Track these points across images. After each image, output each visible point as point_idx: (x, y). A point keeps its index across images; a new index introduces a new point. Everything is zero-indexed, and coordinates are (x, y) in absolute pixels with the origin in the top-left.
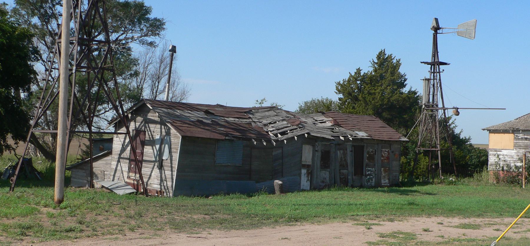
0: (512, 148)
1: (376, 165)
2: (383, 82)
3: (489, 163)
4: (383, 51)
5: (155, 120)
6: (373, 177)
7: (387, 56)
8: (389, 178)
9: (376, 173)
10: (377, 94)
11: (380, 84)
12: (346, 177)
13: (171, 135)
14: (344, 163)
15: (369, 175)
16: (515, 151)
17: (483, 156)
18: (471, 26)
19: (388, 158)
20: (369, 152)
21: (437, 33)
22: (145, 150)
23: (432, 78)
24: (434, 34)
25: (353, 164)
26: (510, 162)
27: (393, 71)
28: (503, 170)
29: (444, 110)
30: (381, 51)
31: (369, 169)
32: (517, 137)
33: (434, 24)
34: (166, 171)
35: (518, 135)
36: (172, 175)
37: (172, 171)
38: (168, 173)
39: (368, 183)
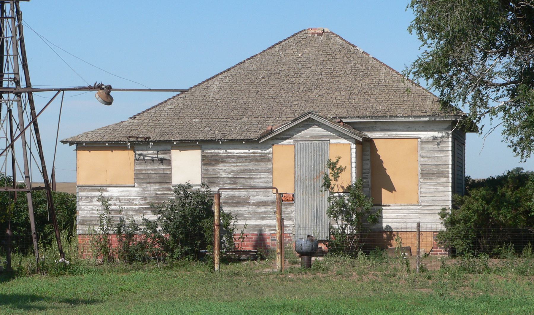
0: (131, 182)
3: (79, 218)
16: (137, 189)
32: (142, 157)
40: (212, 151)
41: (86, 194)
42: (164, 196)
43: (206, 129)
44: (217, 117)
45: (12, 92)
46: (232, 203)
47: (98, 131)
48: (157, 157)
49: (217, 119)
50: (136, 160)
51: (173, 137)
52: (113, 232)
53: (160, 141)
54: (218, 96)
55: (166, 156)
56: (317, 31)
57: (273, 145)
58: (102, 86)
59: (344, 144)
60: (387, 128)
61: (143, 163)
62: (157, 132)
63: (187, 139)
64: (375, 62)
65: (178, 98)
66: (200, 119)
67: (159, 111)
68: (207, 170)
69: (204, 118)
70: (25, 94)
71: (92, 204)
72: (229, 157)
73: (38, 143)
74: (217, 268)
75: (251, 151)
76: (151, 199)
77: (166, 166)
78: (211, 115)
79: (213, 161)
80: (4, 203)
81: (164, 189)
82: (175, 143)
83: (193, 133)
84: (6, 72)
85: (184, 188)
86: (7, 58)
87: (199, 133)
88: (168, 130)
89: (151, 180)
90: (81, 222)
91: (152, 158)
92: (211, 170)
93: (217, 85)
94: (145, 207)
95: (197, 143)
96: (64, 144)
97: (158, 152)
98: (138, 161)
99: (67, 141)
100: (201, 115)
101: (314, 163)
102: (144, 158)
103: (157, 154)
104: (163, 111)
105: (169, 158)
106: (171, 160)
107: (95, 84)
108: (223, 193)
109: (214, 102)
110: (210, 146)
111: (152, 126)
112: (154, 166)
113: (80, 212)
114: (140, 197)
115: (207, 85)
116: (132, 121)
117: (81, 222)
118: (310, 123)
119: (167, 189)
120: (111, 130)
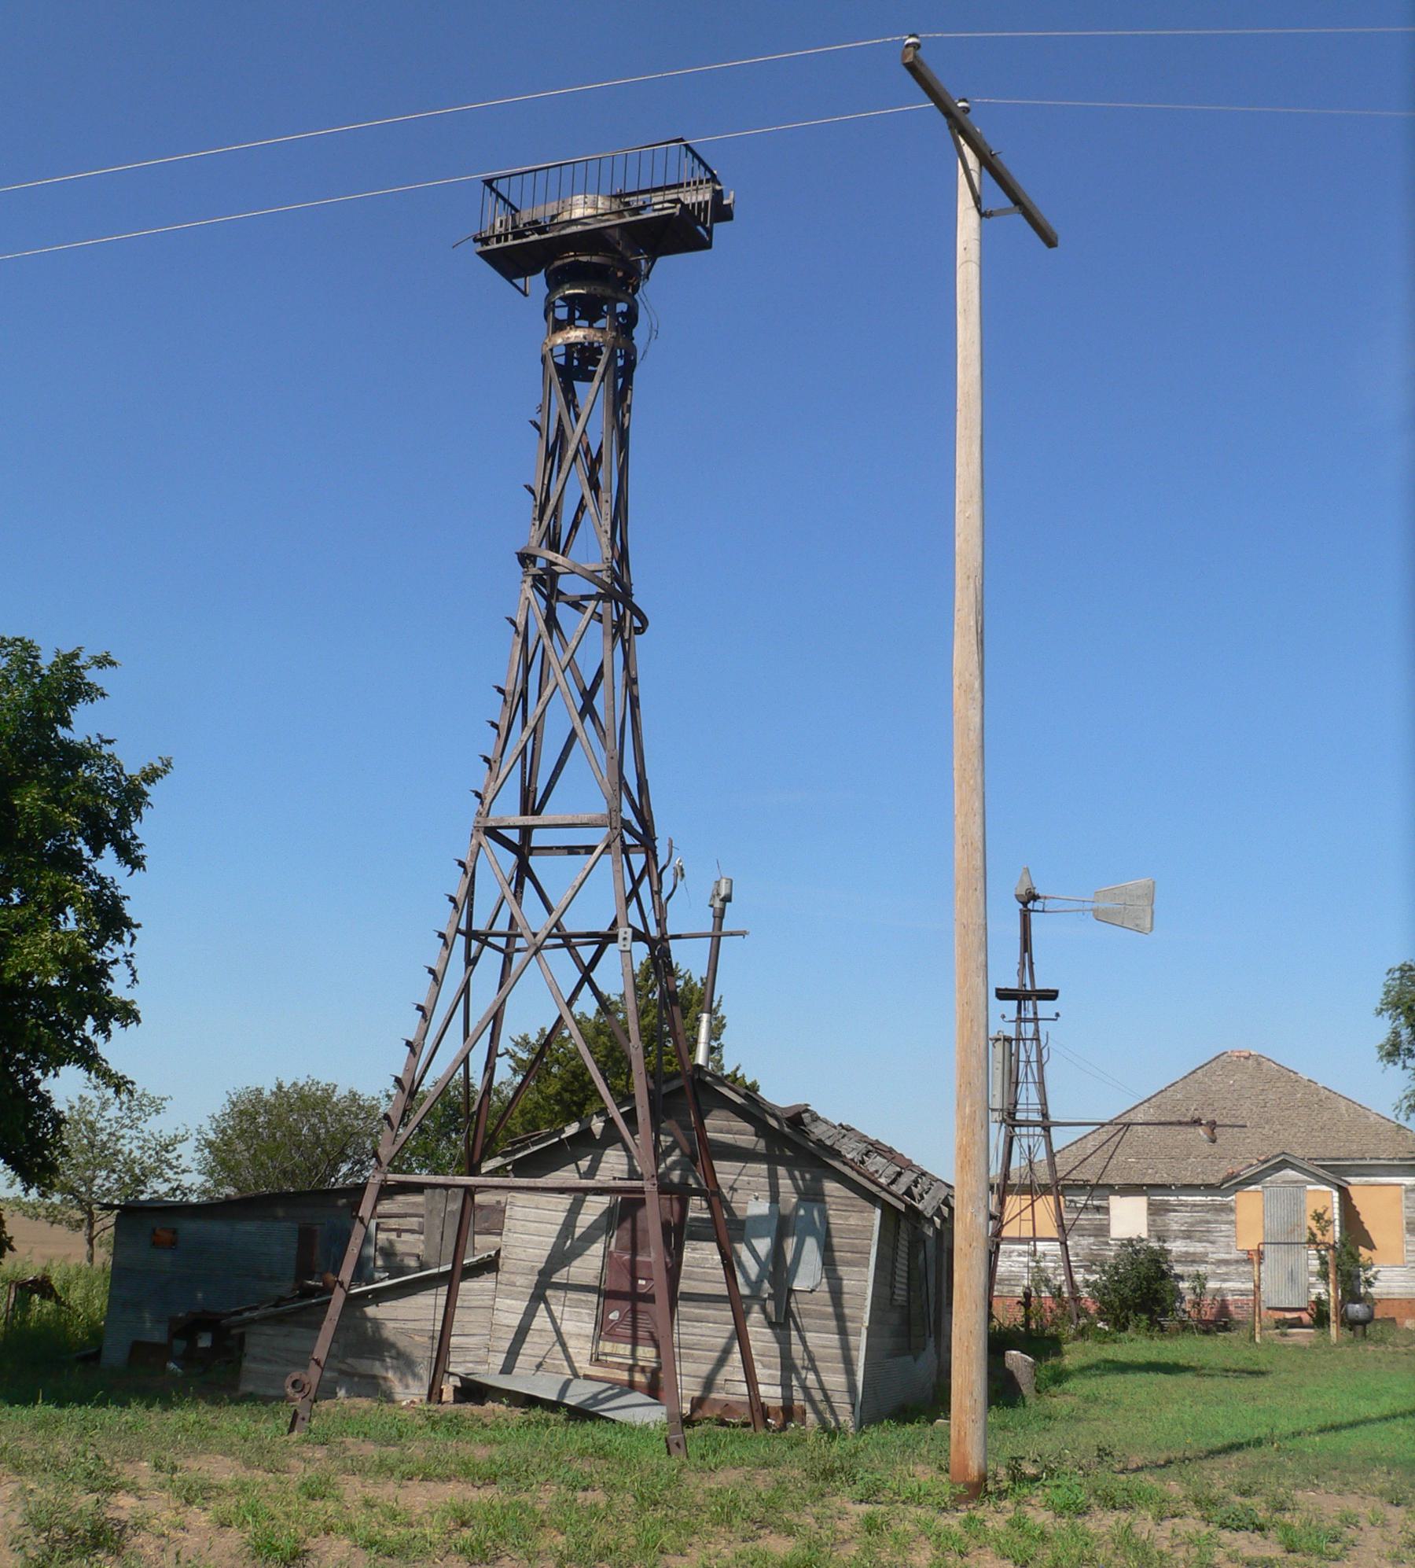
5: (739, 1144)
13: (828, 1199)
22: (686, 1255)
29: (1047, 1129)
32: (1073, 1204)
34: (809, 1335)
35: (1075, 1198)
36: (846, 1349)
37: (843, 1332)
38: (822, 1340)
42: (1101, 1252)
46: (1186, 1261)
55: (1103, 1203)
56: (1243, 1054)
57: (1236, 1191)
59: (1324, 1192)
60: (1365, 1172)
64: (1327, 1092)
68: (1154, 1221)
72: (1182, 1205)
75: (1209, 1198)
89: (1085, 1232)
110: (1160, 1191)
118: (1284, 1165)
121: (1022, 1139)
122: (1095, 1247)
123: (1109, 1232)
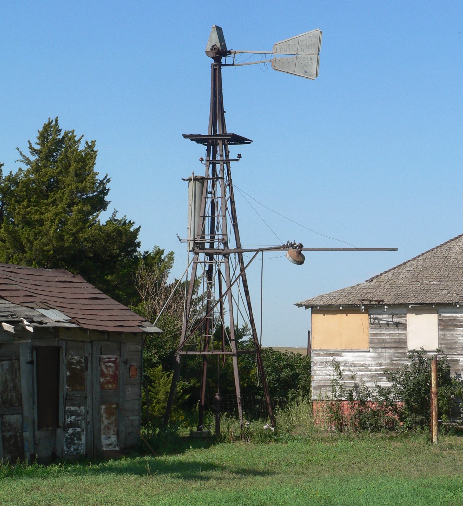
1: (89, 398)
2: (58, 195)
3: (313, 383)
4: (54, 123)
6: (83, 430)
7: (62, 133)
8: (118, 431)
9: (89, 420)
10: (48, 224)
11: (50, 200)
12: (18, 434)
14: (12, 396)
15: (72, 425)
17: (285, 367)
18: (308, 47)
19: (115, 378)
20: (72, 364)
21: (221, 65)
23: (211, 176)
24: (213, 66)
25: (36, 399)
26: (361, 381)
27: (80, 169)
28: (351, 399)
30: (50, 123)
31: (73, 408)
32: (377, 321)
33: (215, 40)
35: (378, 316)
39: (69, 448)
40: (450, 315)
41: (321, 359)
42: (400, 362)
43: (444, 292)
44: (457, 279)
45: (220, 253)
47: (333, 294)
48: (392, 321)
49: (457, 281)
50: (371, 324)
51: (408, 300)
52: (345, 398)
53: (395, 304)
54: (460, 257)
55: (402, 320)
58: (294, 245)
61: (377, 327)
62: (392, 295)
63: (422, 302)
65: (418, 260)
66: (439, 281)
67: (397, 274)
68: (444, 335)
69: (443, 280)
70: (235, 255)
71: (327, 369)
73: (248, 306)
74: (435, 439)
76: (387, 364)
77: (402, 330)
78: (450, 277)
79: (451, 325)
80: (248, 367)
81: (400, 355)
82: (410, 307)
83: (430, 296)
84: (217, 233)
85: (420, 353)
86: (218, 219)
87: (435, 296)
88: (404, 292)
89: (386, 345)
90: (316, 387)
91: (388, 321)
92: (448, 335)
93: (460, 246)
94: (380, 373)
95: (434, 306)
96: (299, 307)
97: (393, 315)
98: (373, 326)
99: (301, 304)
100: (440, 277)
101: (46, 305)
102: (379, 322)
103: (392, 318)
104: (401, 274)
105: (404, 322)
106: (406, 324)
107: (288, 242)
108: (461, 359)
109: (455, 263)
111: (388, 289)
112: (389, 331)
113: (315, 377)
114: (375, 363)
115: (449, 246)
116: (369, 284)
117: (316, 387)
119: (403, 354)
120: (346, 293)
121: (217, 238)
122: (395, 358)
123: (406, 345)
